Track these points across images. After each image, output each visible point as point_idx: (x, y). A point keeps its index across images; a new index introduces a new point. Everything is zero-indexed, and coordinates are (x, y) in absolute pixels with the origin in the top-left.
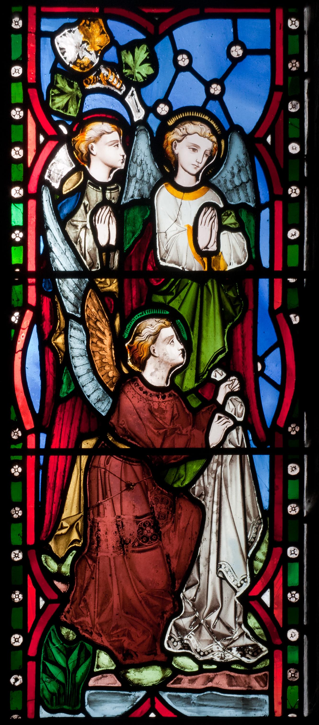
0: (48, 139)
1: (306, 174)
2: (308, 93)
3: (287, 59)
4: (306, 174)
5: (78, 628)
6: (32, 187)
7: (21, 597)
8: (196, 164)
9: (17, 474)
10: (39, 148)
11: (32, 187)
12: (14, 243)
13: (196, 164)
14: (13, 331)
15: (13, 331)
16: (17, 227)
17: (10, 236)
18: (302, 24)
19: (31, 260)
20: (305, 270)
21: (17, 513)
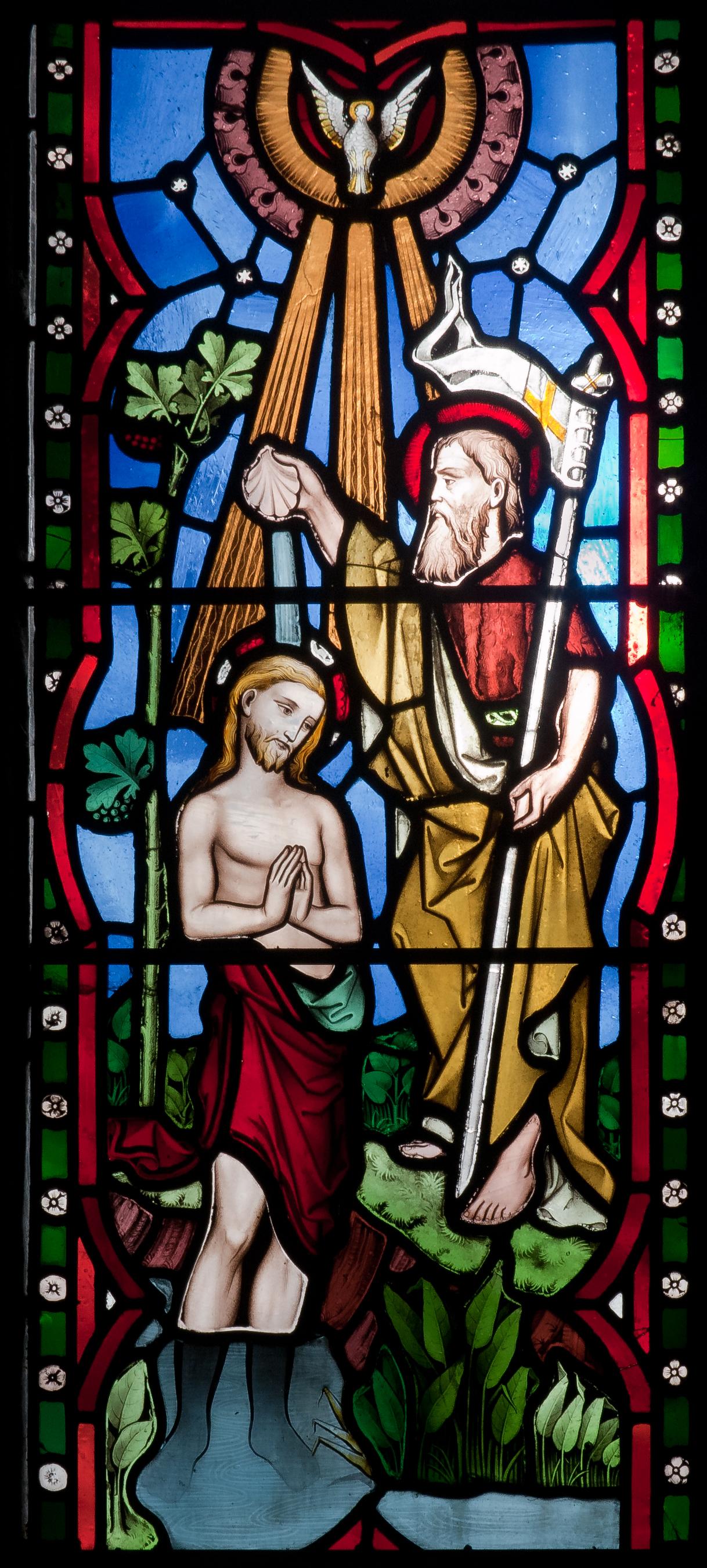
0: (604, 297)
1: (31, 820)
2: (29, 1270)
3: (74, 84)
4: (31, 820)
5: (553, 1348)
6: (639, 1203)
7: (671, 395)
8: (285, 740)
9: (675, 1381)
10: (619, 278)
11: (639, 1203)
12: (677, 131)
13: (285, 740)
14: (680, 894)
15: (680, 894)
16: (669, 332)
17: (685, 402)
18: (42, 157)
19: (639, 531)
20: (32, 344)
21: (675, 1373)
